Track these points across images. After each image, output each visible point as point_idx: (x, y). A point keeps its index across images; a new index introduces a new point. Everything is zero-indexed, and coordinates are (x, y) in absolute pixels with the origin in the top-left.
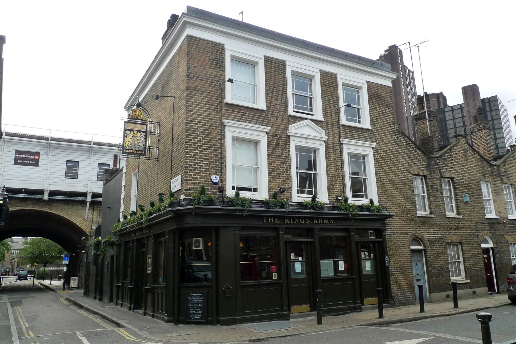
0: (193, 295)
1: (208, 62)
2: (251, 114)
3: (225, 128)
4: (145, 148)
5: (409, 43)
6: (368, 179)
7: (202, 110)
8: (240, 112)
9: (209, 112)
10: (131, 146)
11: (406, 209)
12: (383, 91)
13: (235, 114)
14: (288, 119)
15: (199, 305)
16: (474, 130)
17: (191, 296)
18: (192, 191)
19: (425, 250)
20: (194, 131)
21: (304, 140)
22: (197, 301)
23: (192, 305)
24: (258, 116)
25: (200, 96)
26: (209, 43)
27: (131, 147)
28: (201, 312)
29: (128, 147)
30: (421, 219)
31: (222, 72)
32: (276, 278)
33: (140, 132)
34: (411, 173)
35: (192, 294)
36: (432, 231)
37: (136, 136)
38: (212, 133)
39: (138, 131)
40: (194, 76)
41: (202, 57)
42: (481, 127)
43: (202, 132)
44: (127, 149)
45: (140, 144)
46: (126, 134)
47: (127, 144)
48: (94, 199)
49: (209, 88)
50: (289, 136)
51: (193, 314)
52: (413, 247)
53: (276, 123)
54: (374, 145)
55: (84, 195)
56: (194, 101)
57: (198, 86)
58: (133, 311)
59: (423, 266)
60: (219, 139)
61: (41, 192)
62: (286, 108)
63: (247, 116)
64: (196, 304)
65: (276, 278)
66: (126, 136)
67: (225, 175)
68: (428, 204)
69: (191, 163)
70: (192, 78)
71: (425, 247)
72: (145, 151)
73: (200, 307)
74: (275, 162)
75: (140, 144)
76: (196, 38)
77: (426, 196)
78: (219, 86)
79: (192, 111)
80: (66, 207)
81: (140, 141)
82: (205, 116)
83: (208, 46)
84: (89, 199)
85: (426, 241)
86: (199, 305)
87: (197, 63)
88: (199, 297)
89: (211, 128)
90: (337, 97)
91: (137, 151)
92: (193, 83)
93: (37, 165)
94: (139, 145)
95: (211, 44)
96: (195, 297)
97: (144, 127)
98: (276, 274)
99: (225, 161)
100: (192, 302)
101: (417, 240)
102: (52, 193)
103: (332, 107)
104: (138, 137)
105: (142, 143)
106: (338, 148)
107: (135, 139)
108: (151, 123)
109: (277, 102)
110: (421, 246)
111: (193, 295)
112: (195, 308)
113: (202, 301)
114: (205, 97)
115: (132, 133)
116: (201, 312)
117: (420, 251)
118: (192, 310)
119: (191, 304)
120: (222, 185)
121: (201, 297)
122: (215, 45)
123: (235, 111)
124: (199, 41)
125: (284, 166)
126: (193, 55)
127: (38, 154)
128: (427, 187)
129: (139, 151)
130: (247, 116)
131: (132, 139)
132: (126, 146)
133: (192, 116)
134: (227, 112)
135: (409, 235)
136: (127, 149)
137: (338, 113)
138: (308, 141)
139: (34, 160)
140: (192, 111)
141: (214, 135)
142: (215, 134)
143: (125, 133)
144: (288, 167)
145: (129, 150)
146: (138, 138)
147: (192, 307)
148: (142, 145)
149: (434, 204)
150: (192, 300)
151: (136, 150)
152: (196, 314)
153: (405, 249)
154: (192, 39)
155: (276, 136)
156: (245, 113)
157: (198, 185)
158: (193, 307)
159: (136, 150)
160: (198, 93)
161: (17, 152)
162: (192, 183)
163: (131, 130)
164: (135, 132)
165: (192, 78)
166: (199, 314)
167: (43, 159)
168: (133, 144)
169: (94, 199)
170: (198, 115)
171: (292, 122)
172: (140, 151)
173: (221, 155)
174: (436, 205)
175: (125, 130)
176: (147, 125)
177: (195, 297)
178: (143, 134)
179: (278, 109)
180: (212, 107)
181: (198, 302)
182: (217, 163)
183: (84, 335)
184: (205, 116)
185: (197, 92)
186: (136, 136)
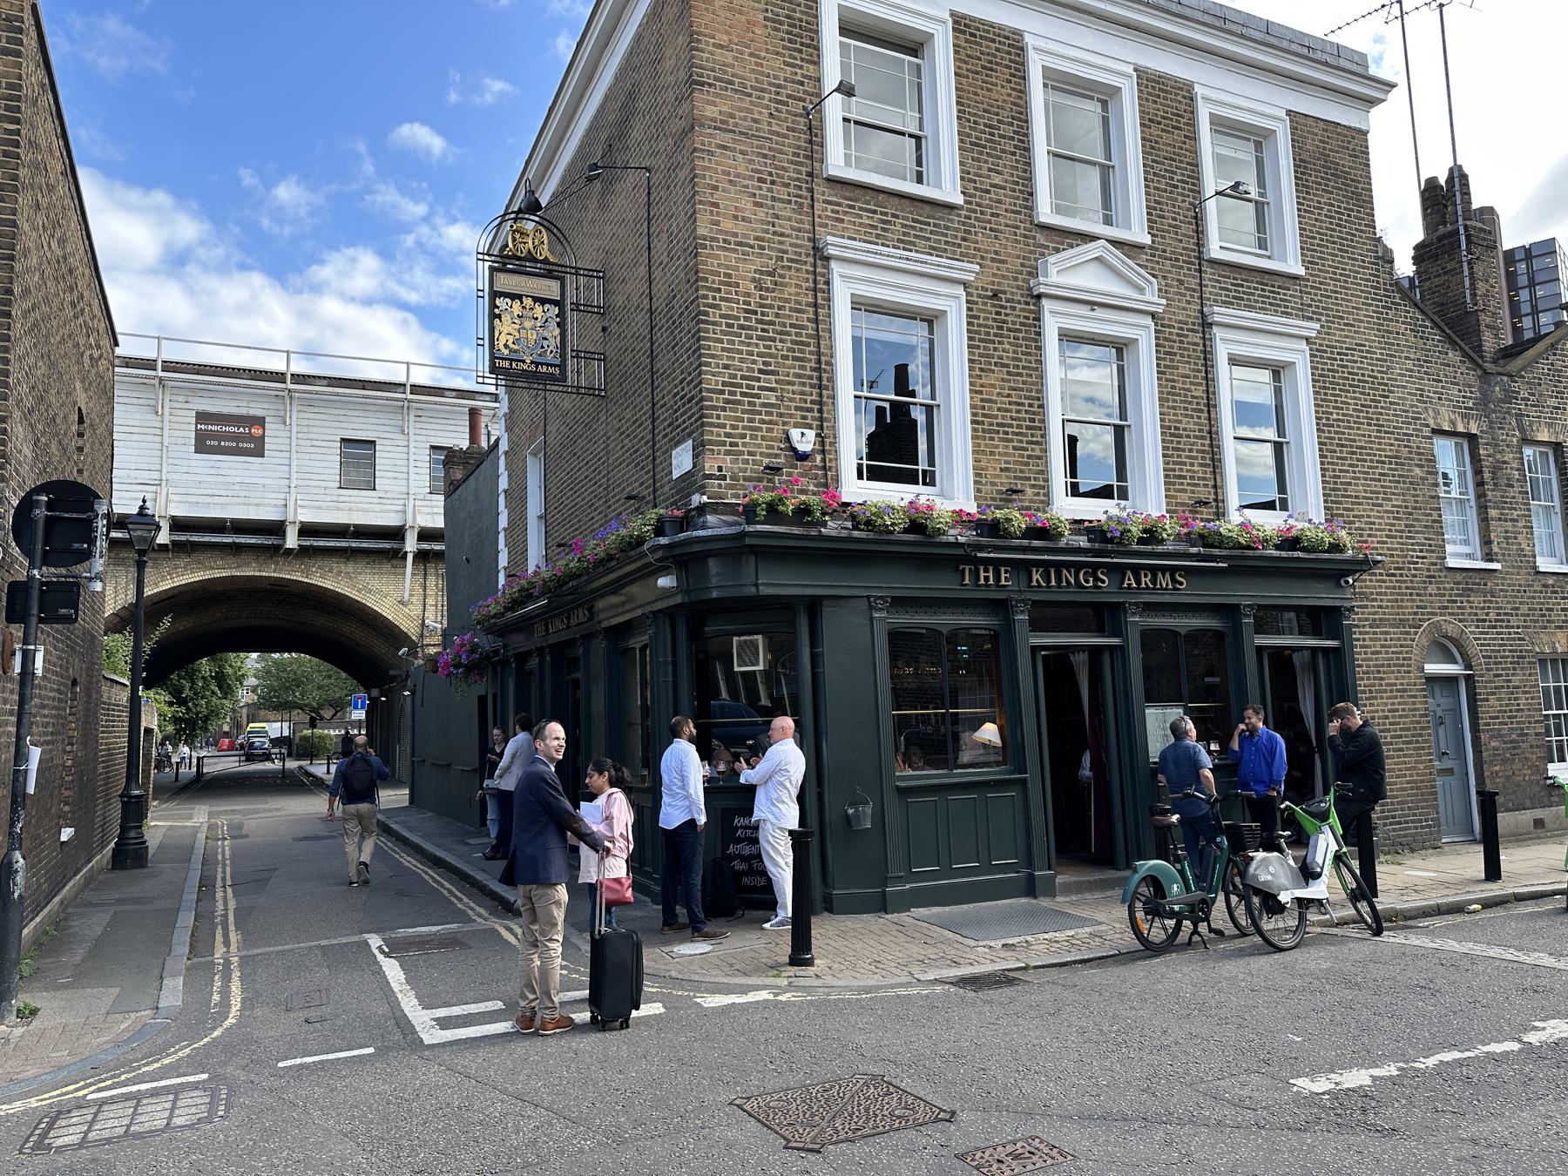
3: (827, 267)
8: (875, 212)
10: (516, 347)
21: (1084, 310)
24: (935, 225)
27: (515, 351)
29: (506, 352)
30: (1459, 577)
39: (536, 299)
40: (716, 79)
45: (545, 343)
48: (426, 546)
50: (1039, 297)
52: (1433, 668)
53: (996, 253)
54: (1312, 328)
55: (397, 533)
57: (732, 116)
60: (808, 305)
61: (277, 528)
66: (499, 317)
70: (710, 85)
71: (1468, 666)
75: (545, 343)
80: (350, 567)
81: (546, 334)
84: (411, 544)
85: (1474, 649)
91: (537, 364)
93: (259, 452)
101: (1445, 647)
102: (306, 530)
106: (1197, 338)
109: (997, 180)
117: (1451, 680)
123: (861, 209)
127: (260, 421)
129: (542, 364)
131: (517, 327)
132: (501, 347)
134: (832, 211)
139: (250, 438)
141: (793, 290)
143: (493, 306)
145: (511, 360)
148: (553, 343)
155: (995, 296)
156: (894, 216)
157: (747, 462)
159: (532, 362)
161: (202, 417)
163: (513, 297)
164: (528, 302)
165: (710, 85)
167: (272, 432)
169: (426, 546)
171: (1047, 247)
172: (548, 365)
175: (494, 295)
182: (807, 389)
183: (395, 949)
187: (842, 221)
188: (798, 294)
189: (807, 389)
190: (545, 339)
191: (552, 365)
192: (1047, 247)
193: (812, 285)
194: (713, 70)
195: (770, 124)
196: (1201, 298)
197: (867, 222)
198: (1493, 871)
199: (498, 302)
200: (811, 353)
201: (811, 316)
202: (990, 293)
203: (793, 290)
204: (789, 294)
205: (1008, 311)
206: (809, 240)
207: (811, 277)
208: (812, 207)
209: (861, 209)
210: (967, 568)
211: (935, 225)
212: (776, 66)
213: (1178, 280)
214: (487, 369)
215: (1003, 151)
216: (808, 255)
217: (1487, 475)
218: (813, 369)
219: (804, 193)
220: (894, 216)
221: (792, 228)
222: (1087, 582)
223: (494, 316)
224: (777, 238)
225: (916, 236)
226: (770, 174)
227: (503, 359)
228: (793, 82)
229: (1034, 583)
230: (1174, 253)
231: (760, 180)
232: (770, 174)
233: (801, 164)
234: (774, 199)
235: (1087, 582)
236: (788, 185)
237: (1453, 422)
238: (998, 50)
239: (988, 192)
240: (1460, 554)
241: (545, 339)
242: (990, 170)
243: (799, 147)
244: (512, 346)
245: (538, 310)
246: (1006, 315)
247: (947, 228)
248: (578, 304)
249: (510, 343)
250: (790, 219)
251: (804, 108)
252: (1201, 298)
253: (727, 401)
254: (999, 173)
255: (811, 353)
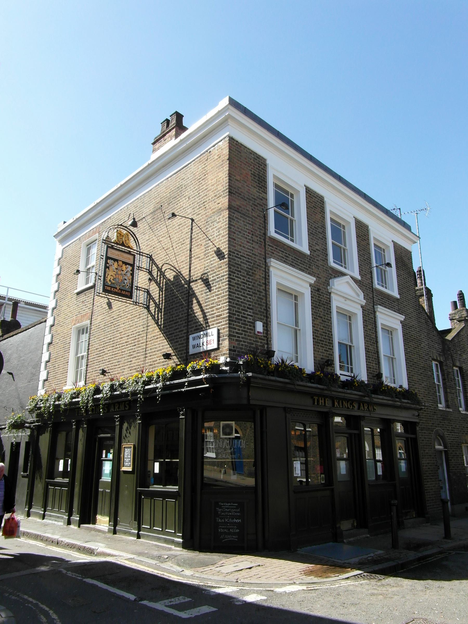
0: (224, 505)
1: (250, 178)
2: (295, 258)
4: (132, 287)
5: (400, 209)
6: (397, 359)
7: (245, 240)
8: (283, 252)
9: (252, 244)
10: (114, 282)
11: (430, 400)
12: (306, 269)
13: (279, 253)
14: (329, 271)
15: (235, 520)
16: (455, 316)
17: (220, 507)
18: (236, 353)
19: (445, 451)
20: (238, 267)
21: (342, 300)
22: (231, 514)
23: (223, 521)
24: (301, 261)
25: (243, 221)
26: (251, 153)
27: (113, 284)
28: (238, 531)
29: (110, 283)
31: (265, 194)
32: (324, 482)
33: (126, 264)
34: (431, 357)
35: (223, 504)
36: (450, 429)
37: (121, 268)
38: (255, 274)
39: (124, 263)
40: (236, 192)
41: (244, 169)
42: (463, 314)
43: (246, 271)
44: (109, 286)
45: (125, 281)
46: (108, 264)
47: (109, 278)
49: (252, 212)
51: (225, 533)
53: (318, 274)
56: (236, 226)
57: (240, 207)
58: (79, 527)
59: (444, 470)
60: (263, 283)
62: (326, 257)
63: (290, 259)
64: (229, 518)
65: (324, 482)
66: (108, 268)
67: (271, 334)
68: (443, 396)
69: (234, 312)
70: (234, 194)
71: (445, 447)
72: (131, 292)
73: (235, 522)
74: (318, 325)
75: (125, 281)
76: (237, 141)
77: (442, 386)
78: (261, 211)
79: (235, 240)
81: (126, 278)
82: (248, 249)
83: (250, 157)
86: (235, 520)
87: (240, 176)
88: (234, 508)
89: (255, 267)
90: (369, 254)
91: (121, 290)
92: (235, 201)
94: (124, 283)
95: (253, 155)
96: (228, 508)
97: (131, 257)
98: (324, 476)
99: (270, 314)
100: (222, 515)
103: (365, 265)
104: (123, 271)
105: (128, 280)
107: (119, 273)
108: (140, 255)
110: (441, 445)
111: (224, 505)
112: (228, 526)
113: (238, 514)
114: (248, 223)
115: (116, 263)
116: (238, 531)
118: (223, 528)
119: (221, 519)
120: (267, 347)
121: (237, 507)
122: (257, 157)
123: (279, 250)
124: (241, 147)
125: (326, 331)
126: (235, 164)
128: (443, 375)
129: (124, 290)
130: (290, 259)
131: (115, 273)
132: (108, 281)
133: (235, 246)
134: (271, 249)
135: (433, 431)
136: (109, 286)
137: (371, 273)
138: (348, 302)
140: (235, 240)
141: (258, 277)
142: (259, 275)
143: (106, 263)
144: (330, 333)
145: (111, 287)
146: (123, 273)
147: (222, 522)
148: (127, 282)
149: (450, 396)
150: (222, 512)
151: (120, 289)
152: (229, 534)
153: (431, 448)
154: (233, 142)
156: (289, 254)
157: (242, 345)
158: (225, 522)
159: (120, 289)
160: (241, 217)
162: (237, 340)
163: (115, 260)
164: (120, 263)
165: (234, 194)
166: (234, 534)
168: (117, 279)
170: (241, 246)
171: (332, 275)
172: (126, 291)
173: (266, 307)
174: (452, 398)
175: (107, 258)
176: (134, 256)
177: (228, 508)
178: (130, 268)
179: (318, 256)
180: (255, 239)
181: (231, 516)
182: (262, 317)
184: (248, 249)
185: (240, 215)
186: (121, 268)
187: (273, 253)
188: (260, 279)
189: (262, 317)
190: (126, 280)
191: (127, 291)
192: (332, 275)
193: (264, 276)
194: (235, 188)
195: (252, 212)
196: (373, 301)
197: (281, 255)
198: (447, 535)
199: (109, 261)
200: (264, 303)
201: (264, 288)
202: (316, 289)
203: (258, 277)
204: (257, 278)
205: (322, 297)
206: (264, 258)
207: (264, 273)
208: (265, 246)
209: (279, 250)
210: (316, 398)
211: (301, 261)
212: (254, 191)
213: (367, 294)
214: (101, 289)
215: (319, 238)
216: (263, 264)
217: (446, 376)
218: (264, 309)
219: (262, 241)
220: (289, 254)
221: (259, 253)
222: (350, 407)
223: (106, 267)
224: (253, 256)
225: (295, 264)
226: (252, 231)
227: (108, 286)
228: (259, 198)
229: (336, 406)
230: (365, 284)
231: (249, 233)
232: (252, 231)
233: (261, 229)
234: (253, 241)
235: (350, 407)
236: (257, 237)
237: (437, 357)
238: (317, 201)
239: (315, 251)
240: (441, 406)
241: (126, 280)
242: (316, 244)
243: (261, 223)
244: (112, 281)
245: (124, 267)
246: (321, 298)
247: (304, 262)
248: (139, 267)
249: (112, 279)
250: (258, 249)
251: (263, 209)
252: (373, 301)
253: (237, 319)
254: (318, 245)
255: (264, 303)
